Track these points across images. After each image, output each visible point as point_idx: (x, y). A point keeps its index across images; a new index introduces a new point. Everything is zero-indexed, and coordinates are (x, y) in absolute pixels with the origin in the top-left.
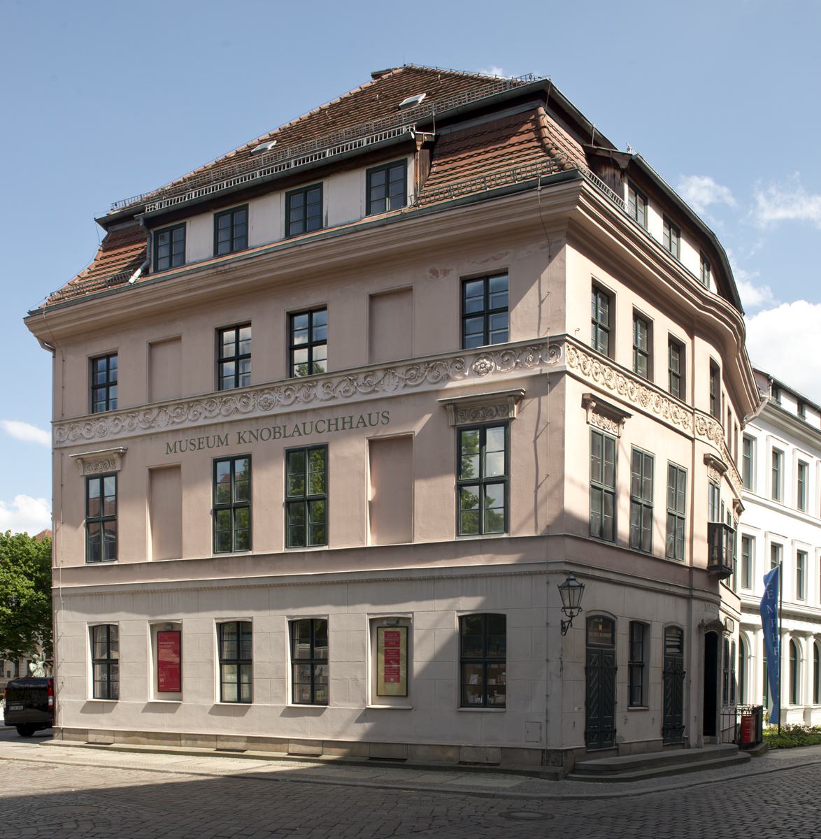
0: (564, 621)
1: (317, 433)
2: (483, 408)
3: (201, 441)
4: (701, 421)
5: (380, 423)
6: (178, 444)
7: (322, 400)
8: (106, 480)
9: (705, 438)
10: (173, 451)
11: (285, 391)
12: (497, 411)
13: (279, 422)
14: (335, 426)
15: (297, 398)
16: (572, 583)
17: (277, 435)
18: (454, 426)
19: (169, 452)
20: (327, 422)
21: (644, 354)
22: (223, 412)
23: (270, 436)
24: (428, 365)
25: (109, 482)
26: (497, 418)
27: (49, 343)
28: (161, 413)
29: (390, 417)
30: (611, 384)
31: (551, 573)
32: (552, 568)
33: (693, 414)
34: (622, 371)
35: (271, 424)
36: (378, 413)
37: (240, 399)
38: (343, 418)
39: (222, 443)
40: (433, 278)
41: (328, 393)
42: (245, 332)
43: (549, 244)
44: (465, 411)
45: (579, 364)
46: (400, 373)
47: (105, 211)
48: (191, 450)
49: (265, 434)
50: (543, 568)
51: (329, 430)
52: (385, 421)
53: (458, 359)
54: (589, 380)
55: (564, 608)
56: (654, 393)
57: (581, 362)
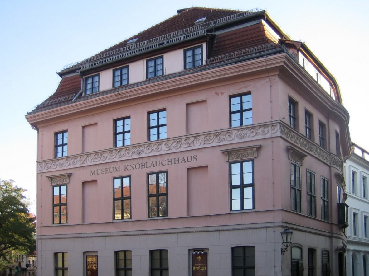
0: (282, 248)
1: (162, 166)
2: (241, 153)
3: (107, 170)
4: (333, 158)
5: (101, 173)
6: (96, 171)
7: (164, 151)
8: (124, 179)
9: (335, 166)
10: (94, 174)
11: (147, 147)
12: (248, 154)
13: (144, 161)
14: (171, 162)
15: (152, 150)
16: (288, 231)
17: (143, 167)
18: (228, 162)
19: (92, 175)
20: (167, 161)
21: (310, 129)
22: (118, 156)
23: (140, 167)
24: (117, 151)
25: (162, 177)
26: (248, 158)
27: (35, 125)
28: (88, 157)
29: (197, 158)
30: (298, 142)
31: (276, 227)
32: (276, 224)
33: (330, 155)
34: (301, 136)
35: (140, 161)
36: (100, 169)
37: (125, 151)
38: (175, 159)
39: (117, 171)
40: (216, 96)
41: (167, 147)
42: (127, 121)
43: (270, 81)
44: (233, 155)
45: (285, 133)
46: (202, 138)
47: (61, 69)
48: (102, 173)
49: (138, 166)
50: (272, 225)
51: (168, 164)
52: (195, 160)
53: (229, 132)
54: (289, 140)
55: (284, 243)
56: (314, 146)
57: (286, 132)
